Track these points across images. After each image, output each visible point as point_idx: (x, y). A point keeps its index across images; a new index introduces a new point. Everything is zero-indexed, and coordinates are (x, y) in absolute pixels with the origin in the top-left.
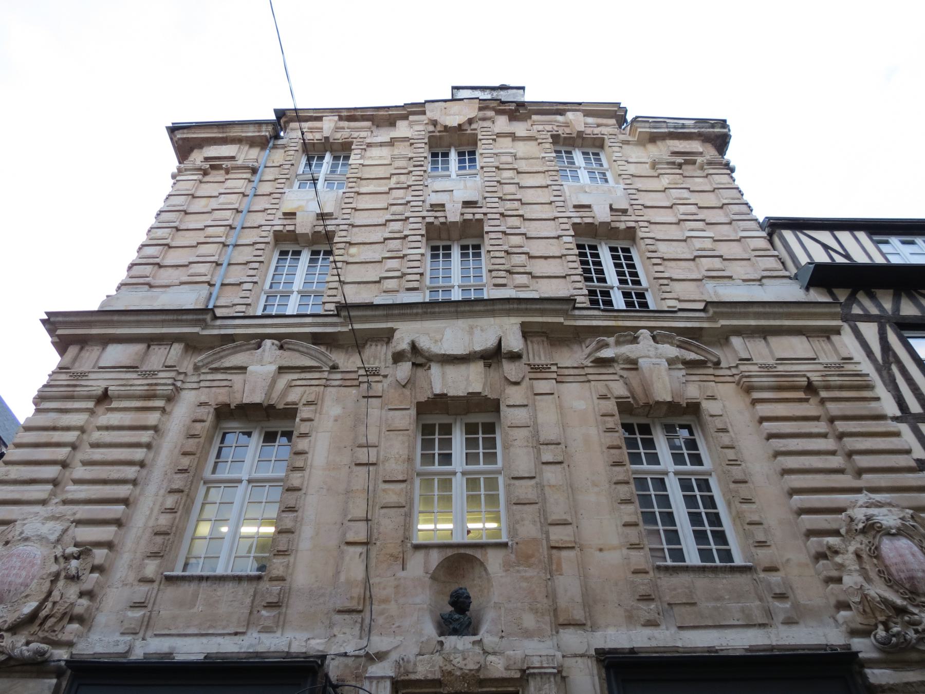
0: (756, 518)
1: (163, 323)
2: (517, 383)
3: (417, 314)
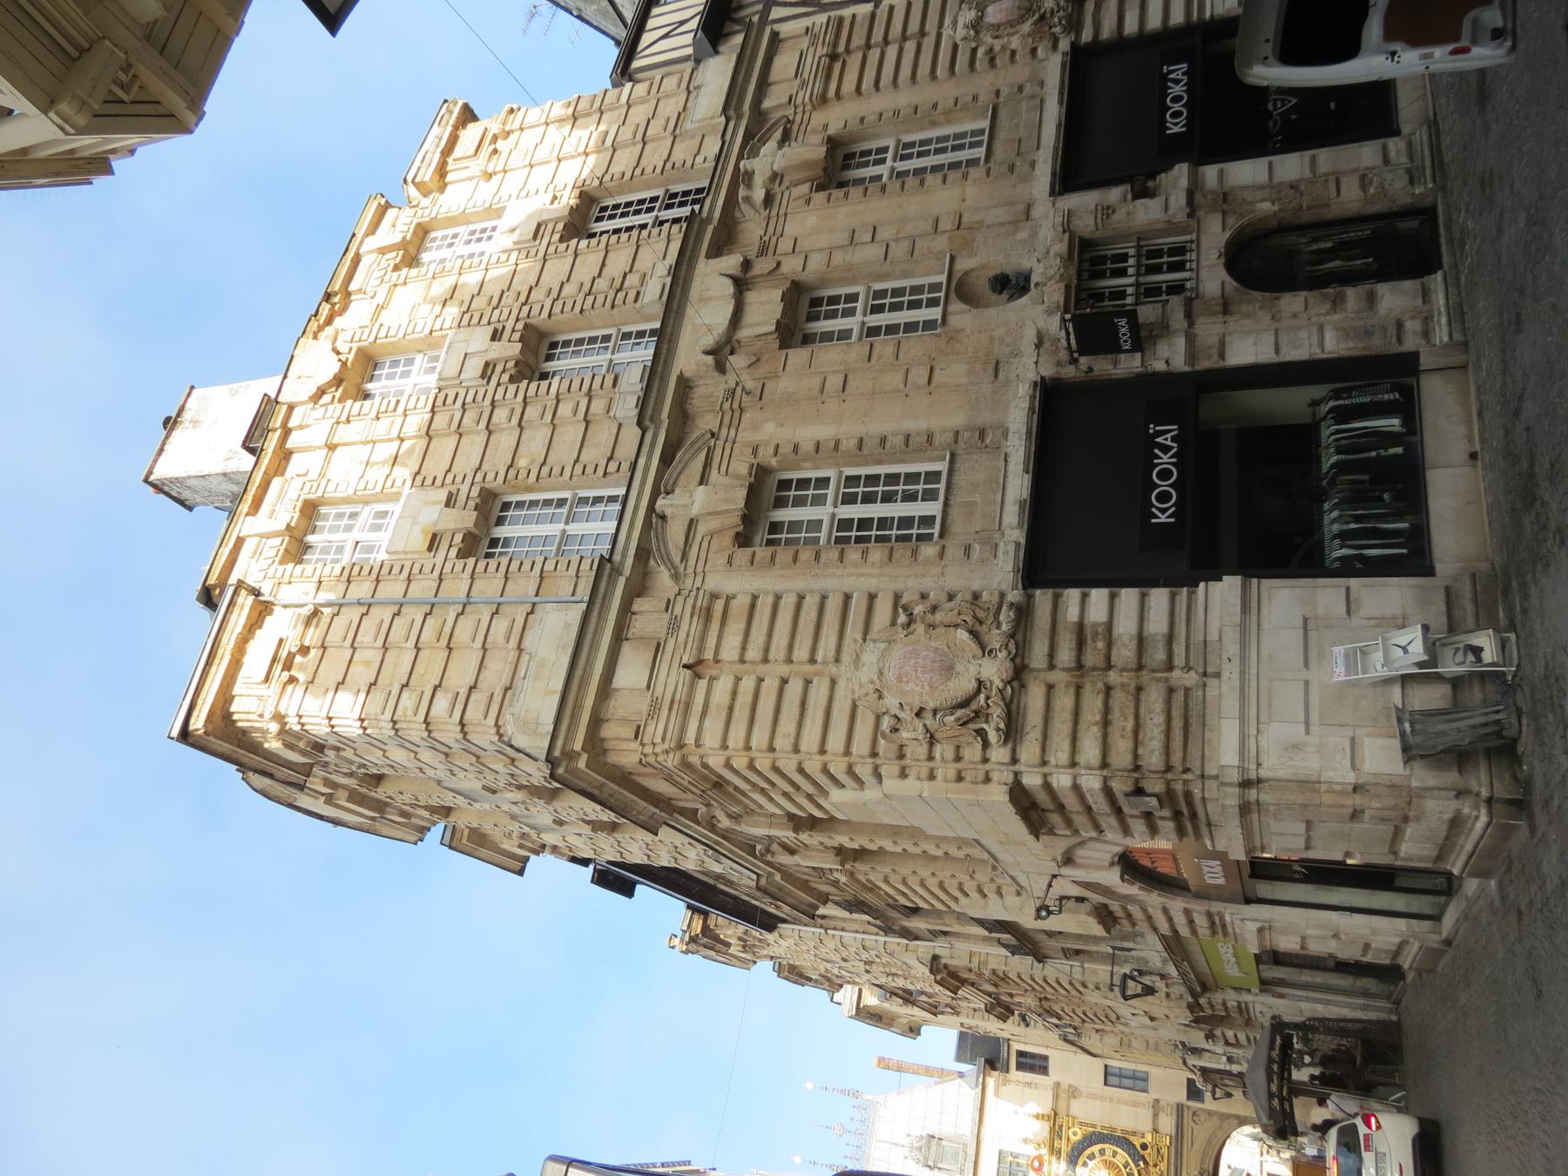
0: (952, 101)
1: (602, 617)
2: (779, 264)
3: (668, 350)
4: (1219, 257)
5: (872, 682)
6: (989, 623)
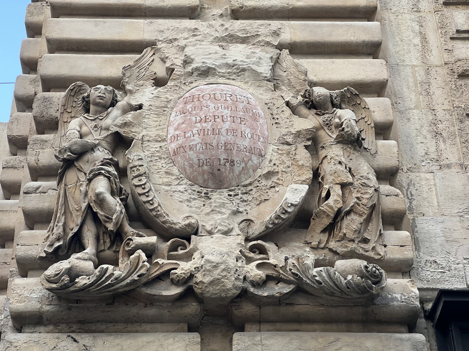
4: (446, 7)
5: (186, 62)
6: (333, 244)
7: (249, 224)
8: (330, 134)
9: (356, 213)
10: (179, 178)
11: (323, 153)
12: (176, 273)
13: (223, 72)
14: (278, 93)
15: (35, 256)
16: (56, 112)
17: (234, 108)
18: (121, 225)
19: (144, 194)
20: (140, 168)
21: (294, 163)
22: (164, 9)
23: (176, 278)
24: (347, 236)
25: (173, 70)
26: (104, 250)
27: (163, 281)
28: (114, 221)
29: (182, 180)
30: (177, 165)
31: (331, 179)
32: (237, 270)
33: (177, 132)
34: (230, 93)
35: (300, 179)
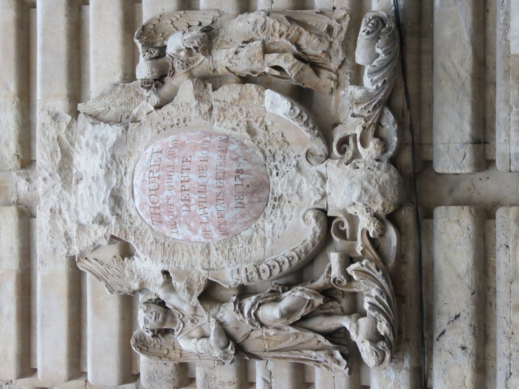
5: (102, 221)
6: (334, 65)
7: (311, 154)
8: (199, 62)
9: (298, 39)
10: (256, 228)
11: (221, 70)
12: (374, 231)
13: (116, 180)
14: (143, 118)
15: (347, 378)
16: (168, 366)
17: (170, 169)
18: (316, 290)
19: (280, 267)
20: (249, 271)
21: (237, 103)
22: (22, 248)
23: (379, 232)
24: (325, 50)
25: (113, 237)
26: (342, 308)
27: (380, 245)
28: (313, 298)
29: (259, 225)
30: (240, 232)
31: (257, 64)
32: (369, 168)
33: (200, 231)
34: (148, 173)
35: (257, 98)
